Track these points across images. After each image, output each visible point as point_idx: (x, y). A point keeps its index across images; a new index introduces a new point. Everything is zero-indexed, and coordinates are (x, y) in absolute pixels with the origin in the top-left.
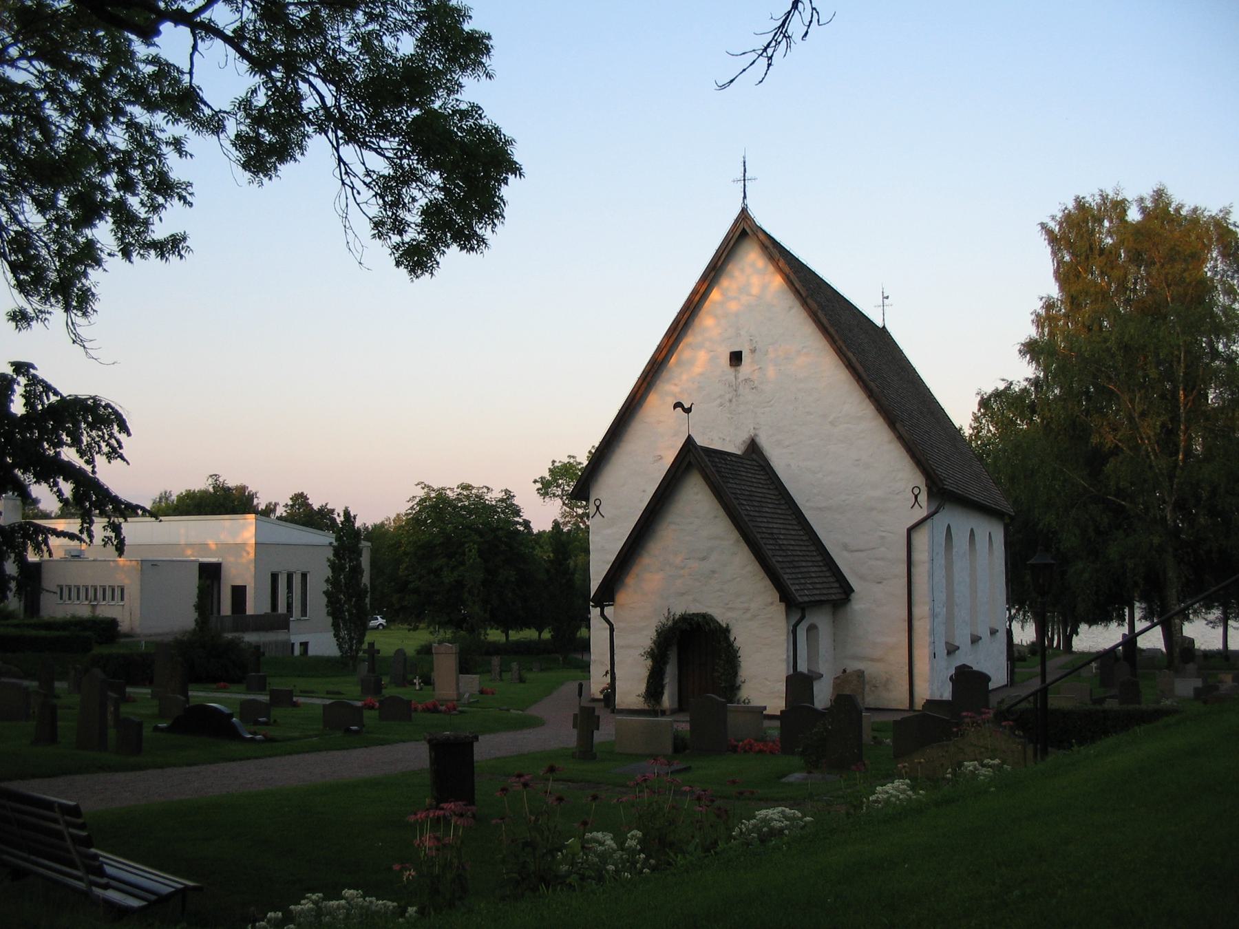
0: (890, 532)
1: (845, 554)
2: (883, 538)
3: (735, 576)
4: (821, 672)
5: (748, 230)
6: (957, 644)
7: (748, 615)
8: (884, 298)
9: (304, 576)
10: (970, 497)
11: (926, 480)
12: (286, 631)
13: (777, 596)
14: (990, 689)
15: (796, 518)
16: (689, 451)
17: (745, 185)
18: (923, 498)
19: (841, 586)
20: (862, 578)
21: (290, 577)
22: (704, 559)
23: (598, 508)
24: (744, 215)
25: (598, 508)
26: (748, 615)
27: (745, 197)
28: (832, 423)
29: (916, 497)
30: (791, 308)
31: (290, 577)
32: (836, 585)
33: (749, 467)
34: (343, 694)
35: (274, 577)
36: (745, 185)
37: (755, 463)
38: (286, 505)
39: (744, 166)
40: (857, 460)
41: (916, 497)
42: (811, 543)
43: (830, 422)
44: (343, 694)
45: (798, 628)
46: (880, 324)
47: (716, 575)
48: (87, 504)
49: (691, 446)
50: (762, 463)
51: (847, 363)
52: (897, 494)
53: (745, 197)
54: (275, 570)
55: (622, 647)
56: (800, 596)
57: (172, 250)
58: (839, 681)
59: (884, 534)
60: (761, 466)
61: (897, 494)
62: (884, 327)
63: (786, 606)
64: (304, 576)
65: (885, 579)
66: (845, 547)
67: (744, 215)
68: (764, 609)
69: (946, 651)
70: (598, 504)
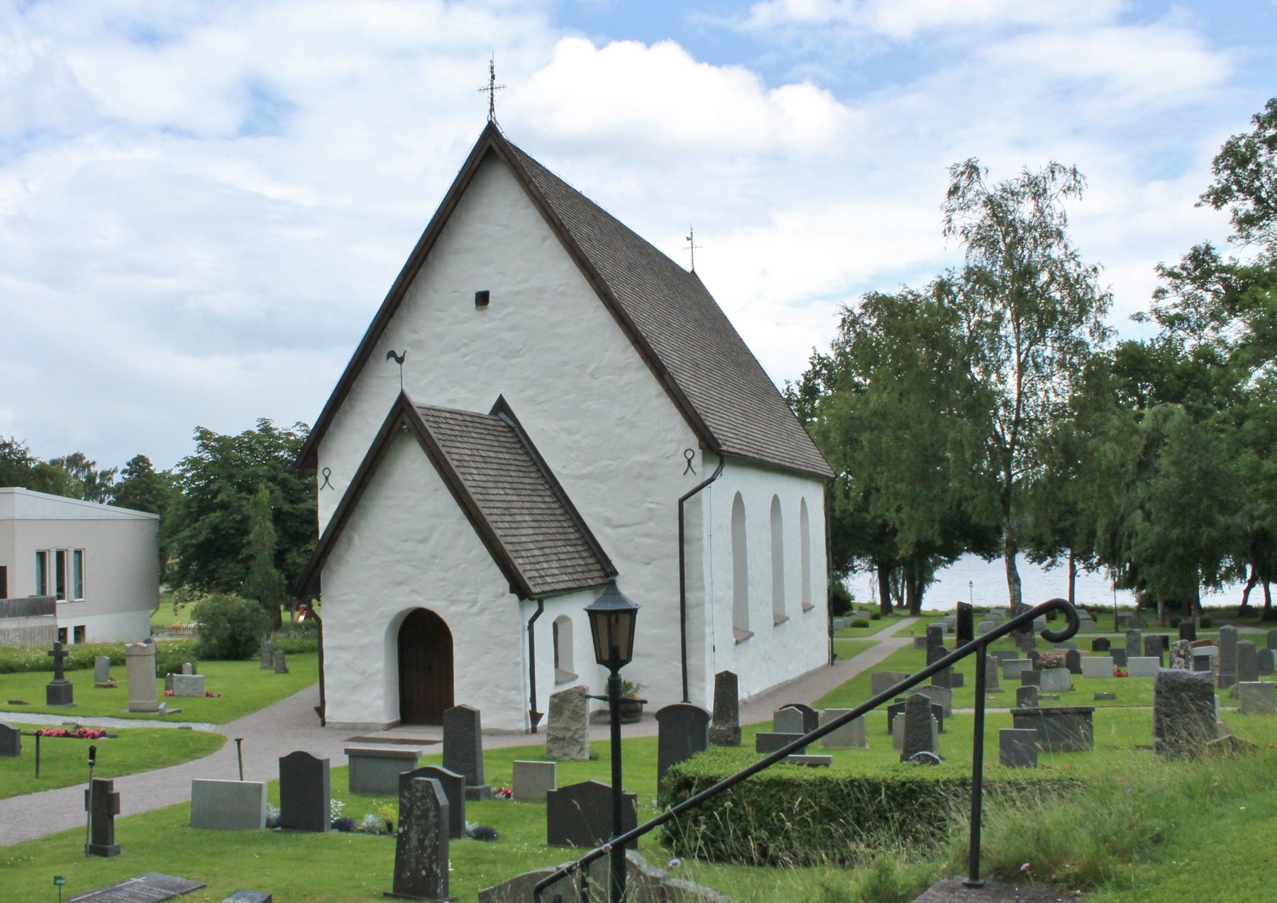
0: (659, 504)
1: (608, 530)
2: (650, 510)
3: (459, 562)
4: (576, 673)
5: (496, 148)
6: (812, 603)
7: (475, 609)
8: (691, 239)
9: (78, 553)
10: (769, 459)
11: (700, 441)
12: (52, 615)
13: (507, 585)
14: (610, 786)
15: (550, 487)
16: (402, 410)
17: (492, 94)
18: (697, 461)
19: (603, 569)
20: (627, 558)
21: (60, 555)
22: (423, 541)
23: (327, 478)
24: (491, 131)
25: (327, 478)
26: (475, 609)
27: (492, 110)
28: (592, 375)
29: (689, 462)
30: (545, 239)
31: (60, 555)
32: (598, 566)
33: (491, 428)
34: (26, 703)
35: (42, 556)
36: (492, 94)
37: (503, 424)
38: (124, 472)
39: (492, 72)
40: (621, 419)
41: (689, 462)
42: (568, 517)
43: (590, 374)
44: (26, 703)
45: (536, 624)
46: (689, 270)
47: (437, 561)
48: (1261, 405)
49: (404, 405)
50: (512, 424)
51: (607, 303)
52: (668, 457)
53: (492, 110)
54: (42, 548)
55: (340, 648)
56: (534, 585)
57: (879, 350)
58: (556, 700)
59: (652, 506)
60: (510, 426)
61: (668, 457)
62: (693, 272)
63: (519, 596)
64: (78, 553)
65: (654, 559)
66: (608, 522)
67: (491, 131)
68: (494, 601)
69: (802, 608)
70: (327, 473)
